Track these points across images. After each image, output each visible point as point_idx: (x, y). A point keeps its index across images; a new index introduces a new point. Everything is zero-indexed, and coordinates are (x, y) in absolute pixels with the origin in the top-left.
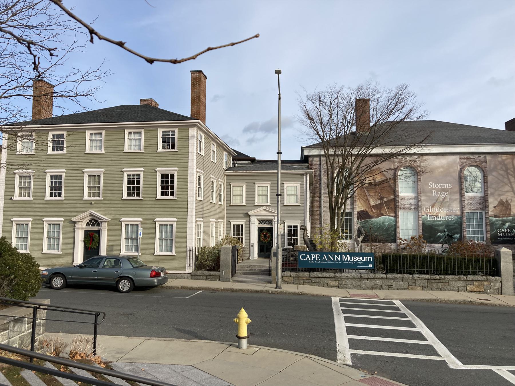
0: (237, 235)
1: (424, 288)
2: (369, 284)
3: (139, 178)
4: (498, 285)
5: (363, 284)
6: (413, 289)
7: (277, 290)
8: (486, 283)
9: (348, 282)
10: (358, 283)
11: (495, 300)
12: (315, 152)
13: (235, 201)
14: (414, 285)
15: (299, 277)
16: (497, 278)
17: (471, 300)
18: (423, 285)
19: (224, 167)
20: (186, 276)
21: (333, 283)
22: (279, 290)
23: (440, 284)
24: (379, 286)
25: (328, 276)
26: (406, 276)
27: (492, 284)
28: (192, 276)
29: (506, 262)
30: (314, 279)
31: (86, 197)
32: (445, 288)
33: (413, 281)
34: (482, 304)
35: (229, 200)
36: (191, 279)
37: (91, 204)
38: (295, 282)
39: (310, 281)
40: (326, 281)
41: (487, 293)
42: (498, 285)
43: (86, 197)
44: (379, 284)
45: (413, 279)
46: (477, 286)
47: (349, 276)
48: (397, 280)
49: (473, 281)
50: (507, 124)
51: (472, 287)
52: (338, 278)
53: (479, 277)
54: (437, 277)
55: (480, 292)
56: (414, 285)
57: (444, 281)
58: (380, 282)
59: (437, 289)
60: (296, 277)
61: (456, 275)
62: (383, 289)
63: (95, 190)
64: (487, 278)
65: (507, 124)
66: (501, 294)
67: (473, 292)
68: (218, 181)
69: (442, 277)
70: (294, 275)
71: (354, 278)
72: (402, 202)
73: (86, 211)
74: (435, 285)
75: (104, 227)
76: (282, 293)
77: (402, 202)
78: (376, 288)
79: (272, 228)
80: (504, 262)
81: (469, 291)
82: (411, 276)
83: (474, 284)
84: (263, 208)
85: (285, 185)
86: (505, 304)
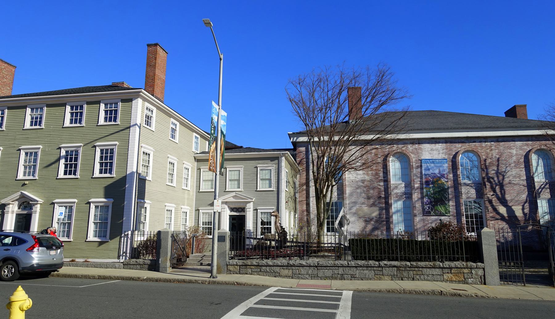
0: (206, 225)
1: (393, 277)
2: (329, 273)
3: (77, 155)
4: (480, 272)
5: (321, 273)
6: (380, 279)
7: (212, 279)
8: (466, 271)
9: (303, 271)
10: (315, 272)
11: (472, 289)
12: (304, 139)
13: (205, 187)
14: (381, 273)
15: (246, 265)
16: (479, 264)
17: (442, 290)
18: (392, 274)
19: (194, 150)
20: (117, 265)
21: (285, 272)
22: (214, 279)
23: (412, 272)
24: (339, 276)
25: (280, 264)
26: (371, 262)
27: (473, 272)
28: (126, 265)
29: (489, 245)
30: (264, 268)
31: (21, 176)
32: (418, 277)
33: (380, 269)
34: (455, 295)
35: (199, 187)
36: (124, 268)
37: (24, 184)
38: (241, 271)
39: (259, 270)
40: (277, 269)
41: (467, 283)
42: (480, 272)
43: (21, 176)
44: (340, 273)
45: (380, 266)
46: (456, 274)
47: (304, 263)
48: (361, 268)
49: (451, 268)
50: (505, 113)
51: (450, 275)
52: (291, 266)
53: (458, 264)
54: (408, 263)
55: (459, 282)
56: (381, 273)
57: (416, 269)
58: (341, 271)
59: (408, 278)
60: (242, 266)
61: (430, 261)
62: (344, 279)
63: (31, 168)
64: (467, 265)
65: (505, 113)
66: (485, 284)
67: (451, 281)
68: (181, 163)
69: (414, 263)
70: (241, 264)
71: (310, 266)
72: (395, 191)
73: (14, 193)
74: (405, 274)
75: (37, 209)
76: (219, 283)
77: (395, 191)
78: (336, 279)
79: (244, 216)
80: (486, 245)
81: (447, 281)
82: (377, 263)
83: (452, 272)
84: (234, 194)
85: (258, 168)
86: (484, 295)
